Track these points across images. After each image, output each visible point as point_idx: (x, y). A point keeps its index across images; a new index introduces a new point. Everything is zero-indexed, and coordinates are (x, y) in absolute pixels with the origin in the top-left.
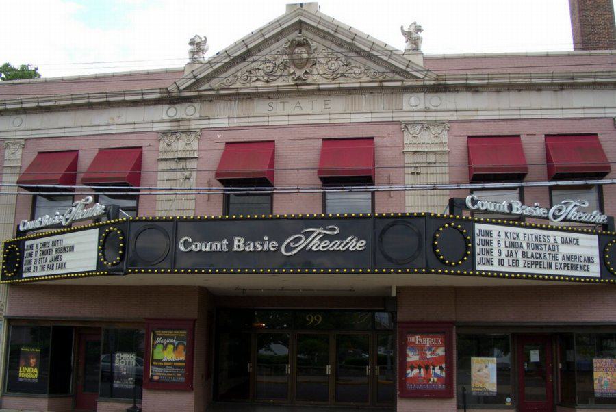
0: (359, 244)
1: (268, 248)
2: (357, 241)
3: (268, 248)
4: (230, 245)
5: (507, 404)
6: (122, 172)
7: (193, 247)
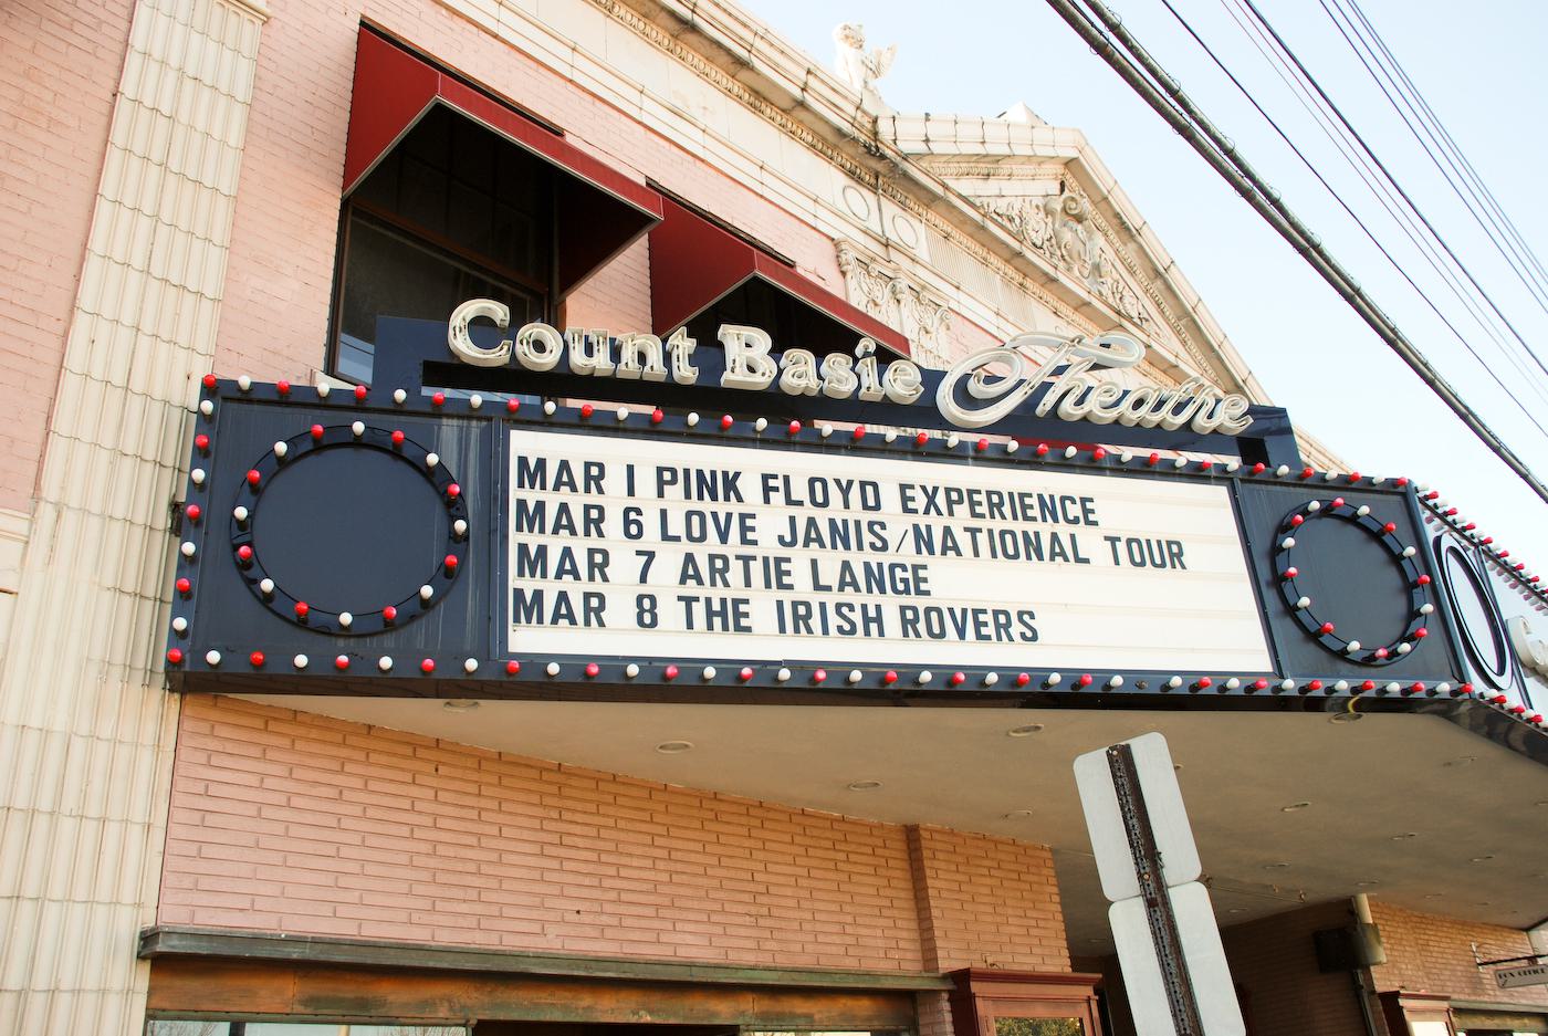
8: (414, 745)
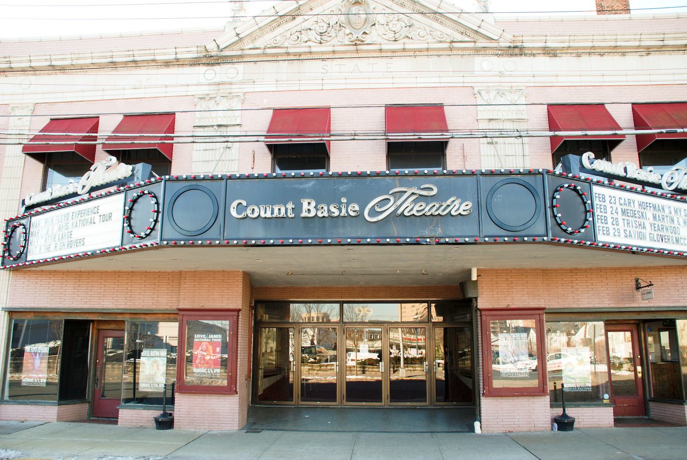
0: (463, 207)
1: (347, 212)
2: (461, 204)
3: (347, 212)
4: (298, 209)
5: (605, 401)
6: (148, 152)
7: (249, 212)
8: (50, 272)
